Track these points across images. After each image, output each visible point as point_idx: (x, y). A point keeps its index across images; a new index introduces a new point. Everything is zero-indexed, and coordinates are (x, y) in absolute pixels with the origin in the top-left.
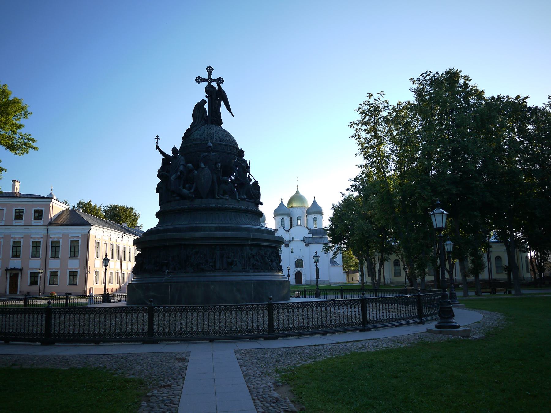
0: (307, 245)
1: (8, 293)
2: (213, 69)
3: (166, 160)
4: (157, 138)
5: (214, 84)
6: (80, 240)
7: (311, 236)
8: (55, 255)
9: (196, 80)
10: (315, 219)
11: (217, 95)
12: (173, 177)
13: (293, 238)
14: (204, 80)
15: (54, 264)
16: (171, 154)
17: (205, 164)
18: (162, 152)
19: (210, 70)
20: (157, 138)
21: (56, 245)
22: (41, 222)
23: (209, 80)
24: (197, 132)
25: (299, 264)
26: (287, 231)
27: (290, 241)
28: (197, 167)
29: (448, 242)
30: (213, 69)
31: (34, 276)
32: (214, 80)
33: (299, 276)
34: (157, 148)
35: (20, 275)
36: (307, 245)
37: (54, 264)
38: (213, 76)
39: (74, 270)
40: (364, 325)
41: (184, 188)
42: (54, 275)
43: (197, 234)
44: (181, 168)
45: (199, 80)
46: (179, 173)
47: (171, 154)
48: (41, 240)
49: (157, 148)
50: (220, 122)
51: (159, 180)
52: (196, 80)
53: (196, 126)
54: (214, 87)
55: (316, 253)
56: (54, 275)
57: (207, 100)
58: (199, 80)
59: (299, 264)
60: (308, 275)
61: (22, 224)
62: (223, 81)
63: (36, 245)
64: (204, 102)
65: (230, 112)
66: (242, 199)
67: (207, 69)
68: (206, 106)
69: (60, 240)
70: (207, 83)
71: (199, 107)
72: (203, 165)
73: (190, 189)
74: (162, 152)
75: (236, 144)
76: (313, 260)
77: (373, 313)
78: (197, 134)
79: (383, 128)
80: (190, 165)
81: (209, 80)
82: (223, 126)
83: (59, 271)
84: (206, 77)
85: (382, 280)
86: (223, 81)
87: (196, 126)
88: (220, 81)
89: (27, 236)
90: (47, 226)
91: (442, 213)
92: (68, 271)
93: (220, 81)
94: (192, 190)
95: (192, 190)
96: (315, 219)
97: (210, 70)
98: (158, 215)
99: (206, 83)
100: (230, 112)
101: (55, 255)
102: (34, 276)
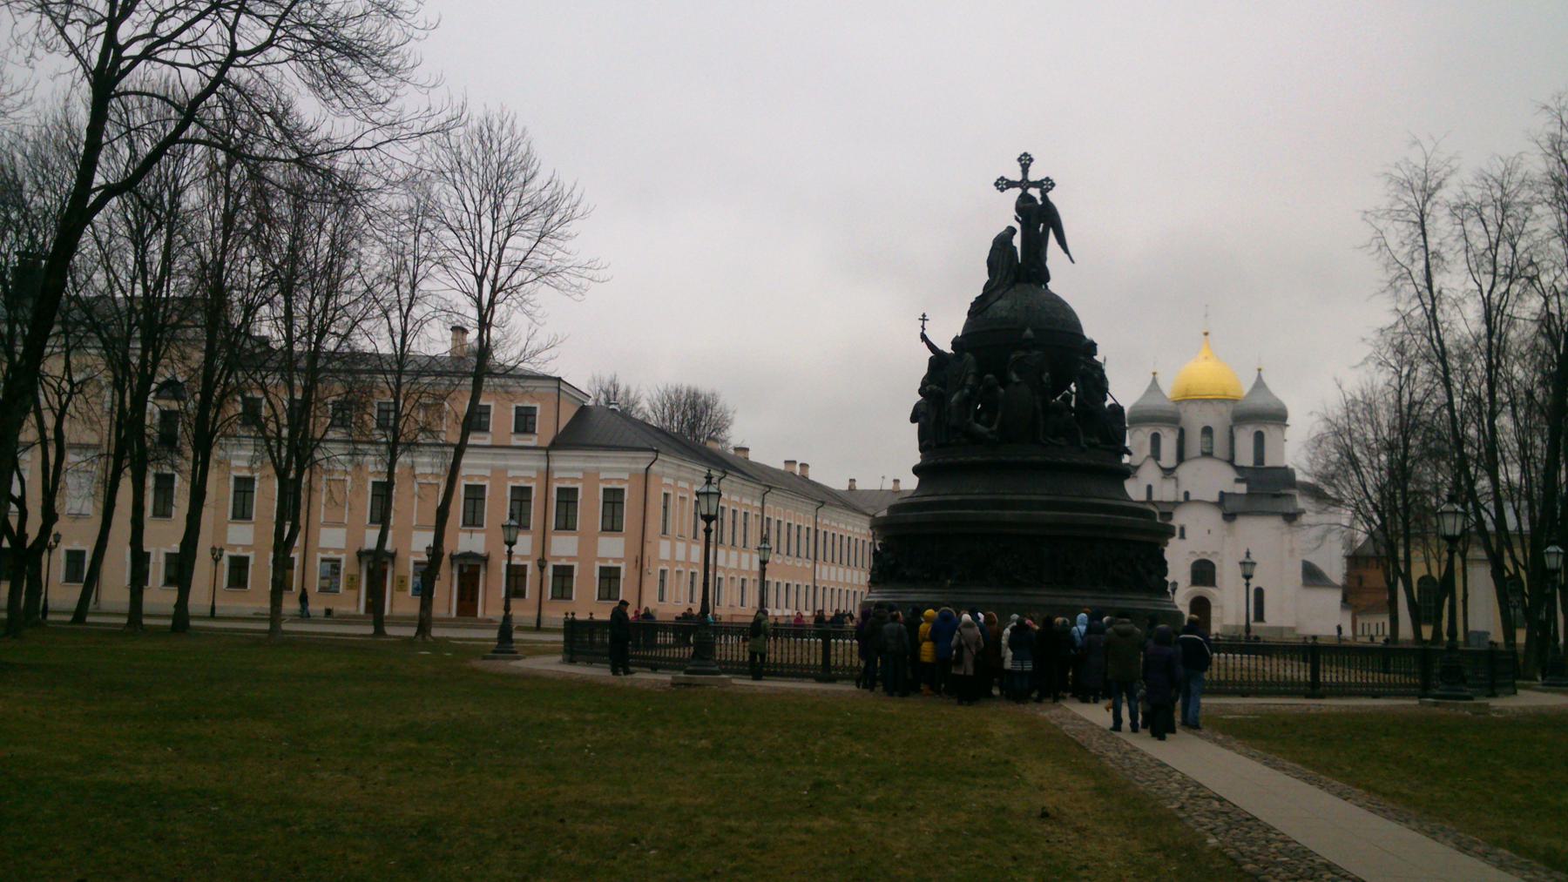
0: (1229, 517)
1: (454, 614)
2: (1031, 160)
3: (938, 361)
4: (924, 318)
5: (1035, 192)
6: (625, 486)
7: (1242, 489)
8: (566, 523)
9: (996, 184)
10: (1259, 438)
11: (1038, 217)
12: (955, 398)
13: (1187, 494)
14: (1012, 184)
15: (564, 547)
16: (948, 349)
17: (1019, 373)
18: (931, 346)
19: (1026, 161)
20: (924, 318)
21: (568, 497)
22: (533, 441)
23: (1025, 184)
24: (999, 303)
25: (1204, 572)
26: (1168, 472)
27: (1176, 504)
28: (1004, 382)
29: (1551, 549)
30: (1031, 160)
31: (563, 577)
32: (1035, 184)
33: (1201, 606)
34: (924, 337)
35: (482, 573)
36: (1229, 517)
37: (564, 547)
38: (1032, 177)
39: (611, 564)
40: (1314, 689)
41: (977, 421)
42: (564, 574)
43: (1008, 514)
44: (970, 381)
45: (1003, 184)
46: (967, 391)
47: (948, 349)
48: (533, 485)
49: (924, 337)
50: (1045, 277)
51: (919, 398)
52: (996, 184)
53: (997, 288)
54: (1033, 199)
55: (1248, 554)
56: (564, 574)
57: (1017, 226)
58: (1003, 184)
59: (1204, 572)
60: (1228, 611)
61: (488, 442)
62: (1053, 185)
63: (521, 496)
64: (1012, 231)
65: (1066, 251)
66: (1094, 446)
67: (1020, 160)
68: (1017, 241)
69: (579, 485)
70: (1018, 191)
71: (1002, 244)
72: (1014, 377)
73: (988, 424)
74: (931, 346)
75: (1077, 325)
76: (1239, 571)
77: (1328, 675)
78: (1001, 306)
79: (1442, 227)
80: (989, 376)
81: (1025, 184)
82: (1053, 286)
83: (576, 565)
84: (1018, 177)
85: (1460, 636)
86: (1053, 185)
87: (997, 288)
88: (1046, 185)
89: (500, 473)
90: (547, 449)
91: (1456, 512)
92: (598, 564)
93: (1046, 185)
94: (995, 427)
95: (995, 427)
96: (1259, 438)
97: (1026, 161)
98: (917, 470)
99: (1018, 191)
100: (1066, 251)
101: (566, 523)
102: (563, 577)
